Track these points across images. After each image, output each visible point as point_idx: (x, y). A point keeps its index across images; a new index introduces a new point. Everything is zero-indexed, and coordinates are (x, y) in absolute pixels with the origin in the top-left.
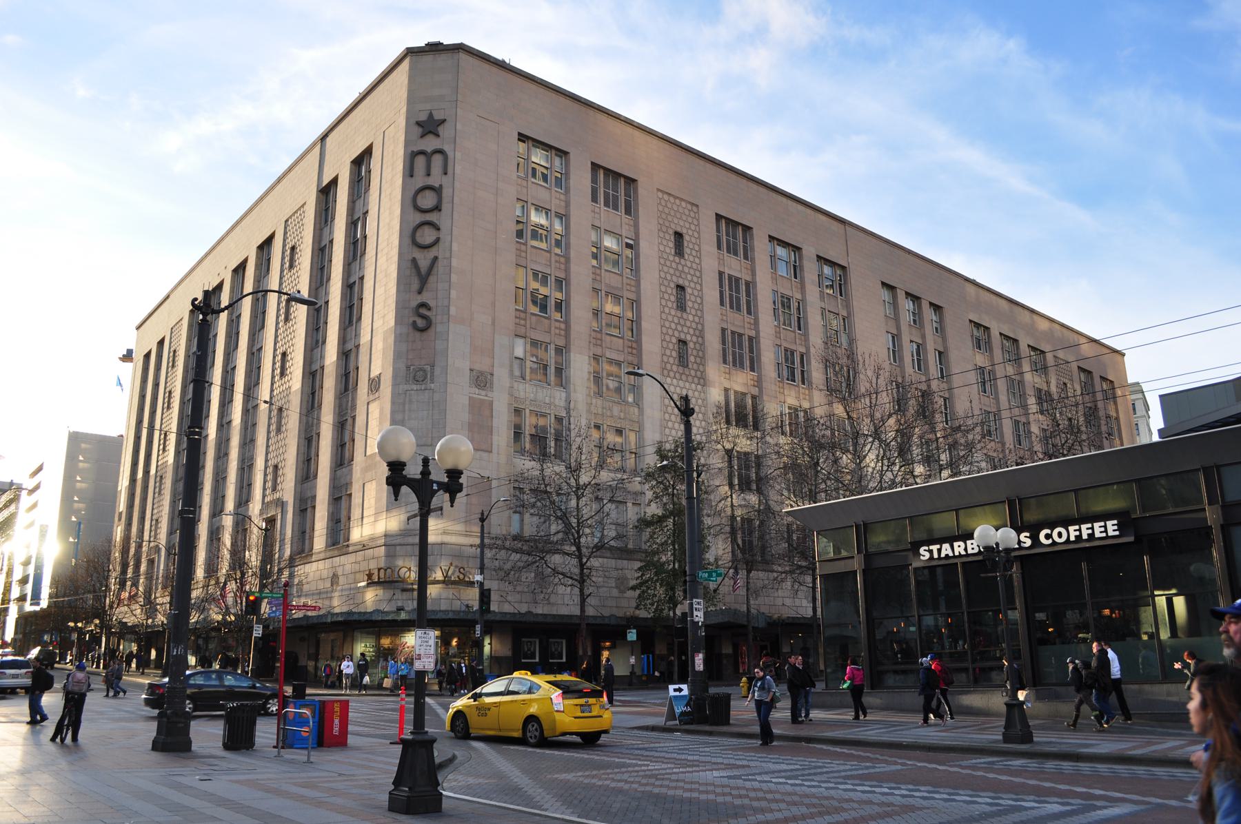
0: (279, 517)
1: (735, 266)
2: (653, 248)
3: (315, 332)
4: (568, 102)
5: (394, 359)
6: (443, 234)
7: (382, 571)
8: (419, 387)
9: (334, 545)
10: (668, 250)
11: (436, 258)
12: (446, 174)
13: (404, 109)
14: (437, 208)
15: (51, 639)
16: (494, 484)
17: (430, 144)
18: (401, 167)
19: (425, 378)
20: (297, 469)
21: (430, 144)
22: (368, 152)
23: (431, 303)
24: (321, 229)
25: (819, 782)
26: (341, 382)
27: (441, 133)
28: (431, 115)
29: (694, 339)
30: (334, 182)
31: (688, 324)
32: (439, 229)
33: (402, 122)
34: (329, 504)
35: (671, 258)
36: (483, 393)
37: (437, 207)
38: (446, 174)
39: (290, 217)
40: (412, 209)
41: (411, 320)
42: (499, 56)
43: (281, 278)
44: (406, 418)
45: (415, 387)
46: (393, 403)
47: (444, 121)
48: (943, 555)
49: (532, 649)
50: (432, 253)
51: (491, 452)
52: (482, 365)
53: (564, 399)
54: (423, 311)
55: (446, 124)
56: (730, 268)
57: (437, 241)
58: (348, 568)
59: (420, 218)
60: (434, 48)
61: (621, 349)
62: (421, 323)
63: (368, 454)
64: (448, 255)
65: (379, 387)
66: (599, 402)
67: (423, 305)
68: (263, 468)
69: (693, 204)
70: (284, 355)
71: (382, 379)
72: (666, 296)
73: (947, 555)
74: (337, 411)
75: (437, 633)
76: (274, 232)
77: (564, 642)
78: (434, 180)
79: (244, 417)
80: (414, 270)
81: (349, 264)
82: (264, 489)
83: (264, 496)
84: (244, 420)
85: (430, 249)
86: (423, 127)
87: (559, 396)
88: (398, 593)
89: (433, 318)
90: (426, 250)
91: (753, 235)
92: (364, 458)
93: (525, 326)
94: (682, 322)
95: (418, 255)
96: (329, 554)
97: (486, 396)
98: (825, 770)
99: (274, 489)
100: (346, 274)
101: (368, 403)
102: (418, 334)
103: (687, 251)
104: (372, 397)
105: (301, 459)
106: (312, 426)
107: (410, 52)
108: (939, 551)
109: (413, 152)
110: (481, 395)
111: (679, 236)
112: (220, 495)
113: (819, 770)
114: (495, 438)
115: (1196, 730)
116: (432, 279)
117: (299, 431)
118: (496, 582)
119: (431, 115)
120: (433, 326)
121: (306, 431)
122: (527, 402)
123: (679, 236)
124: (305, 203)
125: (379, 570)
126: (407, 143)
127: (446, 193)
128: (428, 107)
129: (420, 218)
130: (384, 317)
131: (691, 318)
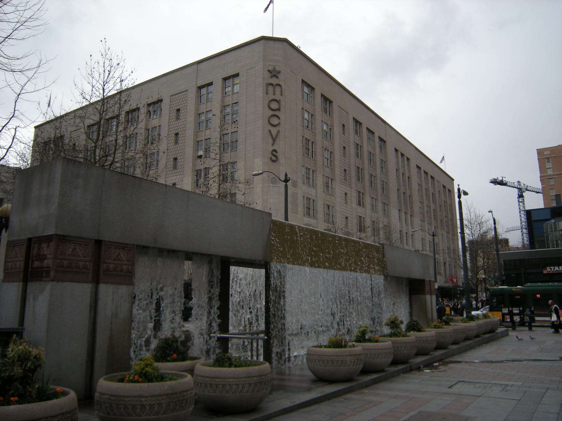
2: (337, 130)
4: (316, 69)
10: (341, 132)
14: (279, 109)
17: (274, 81)
21: (274, 81)
23: (278, 150)
27: (268, 73)
28: (274, 68)
32: (279, 119)
38: (281, 95)
42: (296, 44)
45: (272, 185)
48: (555, 270)
50: (276, 129)
51: (297, 213)
54: (274, 153)
62: (274, 158)
67: (275, 151)
73: (557, 270)
80: (269, 135)
86: (271, 73)
87: (314, 191)
95: (272, 129)
102: (274, 163)
103: (346, 132)
108: (554, 269)
111: (344, 125)
116: (278, 140)
119: (274, 68)
123: (344, 125)
127: (282, 103)
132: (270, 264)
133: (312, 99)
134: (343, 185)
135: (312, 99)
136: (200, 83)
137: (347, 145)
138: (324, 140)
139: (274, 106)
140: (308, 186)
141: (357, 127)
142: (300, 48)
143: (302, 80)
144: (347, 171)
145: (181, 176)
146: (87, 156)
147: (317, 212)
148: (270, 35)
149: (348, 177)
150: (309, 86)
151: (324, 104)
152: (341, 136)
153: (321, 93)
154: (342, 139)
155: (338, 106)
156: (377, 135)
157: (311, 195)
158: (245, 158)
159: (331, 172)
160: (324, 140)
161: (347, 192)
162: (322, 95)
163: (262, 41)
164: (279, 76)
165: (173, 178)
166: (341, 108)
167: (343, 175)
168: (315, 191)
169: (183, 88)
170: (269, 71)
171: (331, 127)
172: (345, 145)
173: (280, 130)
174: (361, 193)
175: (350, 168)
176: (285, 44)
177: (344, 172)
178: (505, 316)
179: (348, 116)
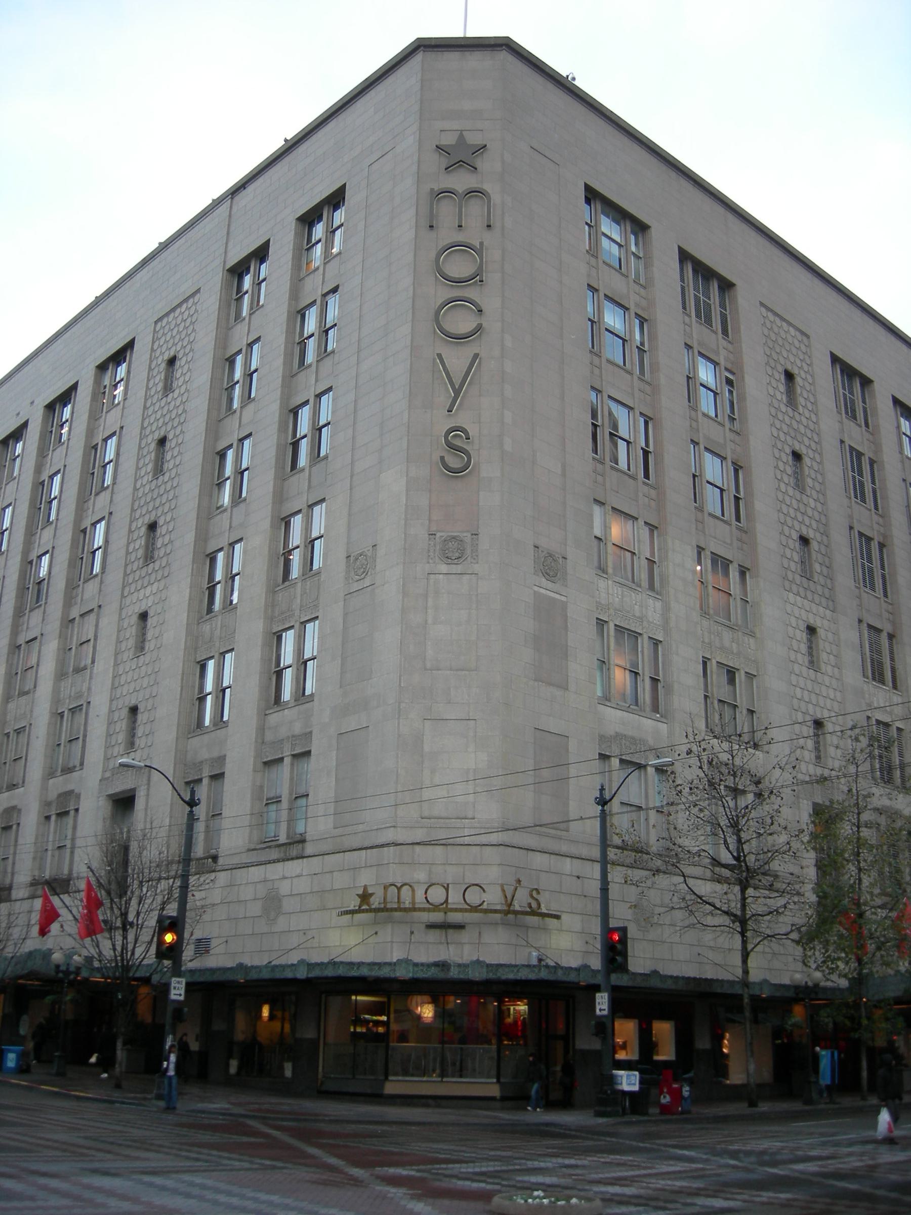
1: (856, 436)
10: (779, 396)
17: (461, 181)
23: (472, 431)
28: (461, 137)
29: (818, 535)
31: (810, 512)
35: (783, 409)
42: (562, 68)
44: (430, 621)
45: (444, 568)
51: (566, 689)
58: (303, 886)
61: (728, 541)
62: (454, 462)
66: (705, 623)
69: (803, 333)
72: (781, 465)
78: (474, 234)
87: (653, 609)
94: (802, 507)
99: (131, 744)
103: (801, 400)
109: (432, 190)
110: (546, 589)
111: (789, 376)
115: (385, 999)
119: (461, 137)
122: (612, 611)
123: (789, 376)
124: (198, 291)
127: (493, 255)
128: (456, 125)
132: (219, 836)
133: (641, 262)
134: (798, 594)
135: (641, 262)
136: (235, 257)
137: (809, 447)
138: (864, 595)
140: (630, 584)
142: (574, 79)
143: (588, 188)
144: (814, 545)
145: (163, 583)
147: (669, 690)
148: (455, 32)
149: (817, 567)
150: (620, 215)
152: (778, 409)
153: (680, 249)
155: (762, 304)
157: (641, 619)
158: (352, 477)
159: (739, 540)
160: (864, 595)
161: (817, 622)
163: (419, 57)
165: (148, 591)
167: (796, 557)
168: (659, 604)
169: (187, 288)
171: (733, 373)
172: (797, 447)
174: (884, 635)
175: (826, 534)
176: (504, 56)
177: (797, 544)
178: (767, 1075)
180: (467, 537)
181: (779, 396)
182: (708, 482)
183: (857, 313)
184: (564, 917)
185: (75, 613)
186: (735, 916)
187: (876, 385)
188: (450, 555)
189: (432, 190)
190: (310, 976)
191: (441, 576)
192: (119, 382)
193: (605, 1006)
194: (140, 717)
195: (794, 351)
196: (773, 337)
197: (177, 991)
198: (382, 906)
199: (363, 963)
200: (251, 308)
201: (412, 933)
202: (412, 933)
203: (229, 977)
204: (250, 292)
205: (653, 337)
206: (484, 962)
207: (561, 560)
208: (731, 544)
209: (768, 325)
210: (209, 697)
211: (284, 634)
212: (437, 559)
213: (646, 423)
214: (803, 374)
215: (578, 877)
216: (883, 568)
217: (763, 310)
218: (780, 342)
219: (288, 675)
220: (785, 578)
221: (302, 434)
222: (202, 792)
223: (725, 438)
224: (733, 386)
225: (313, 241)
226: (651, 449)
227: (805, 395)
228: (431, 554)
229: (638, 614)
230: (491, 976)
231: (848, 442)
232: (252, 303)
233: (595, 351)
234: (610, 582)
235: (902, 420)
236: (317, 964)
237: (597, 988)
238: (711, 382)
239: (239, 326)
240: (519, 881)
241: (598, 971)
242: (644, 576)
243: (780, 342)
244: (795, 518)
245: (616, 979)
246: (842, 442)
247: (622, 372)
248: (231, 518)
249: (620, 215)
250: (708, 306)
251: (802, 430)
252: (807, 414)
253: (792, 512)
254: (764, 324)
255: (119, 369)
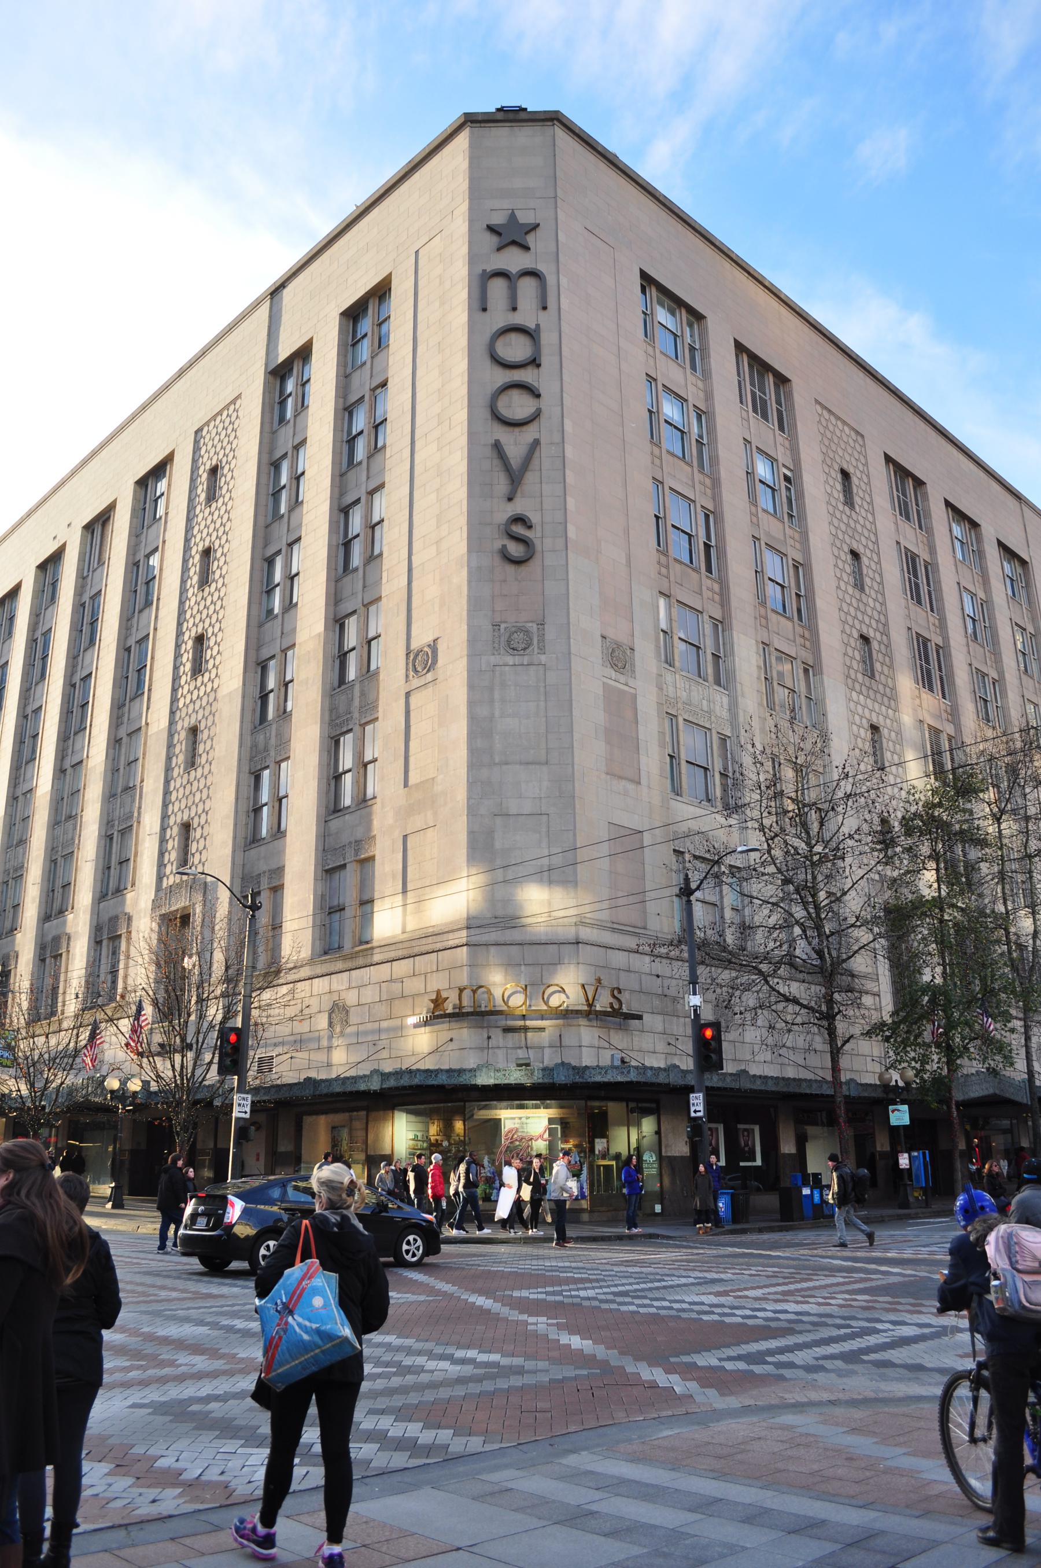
0: (198, 909)
3: (265, 595)
5: (469, 611)
6: (547, 402)
7: (467, 994)
8: (517, 660)
9: (326, 953)
10: (836, 495)
11: (536, 443)
12: (545, 308)
13: (465, 207)
14: (534, 362)
15: (1005, 1132)
16: (647, 838)
17: (514, 261)
18: (464, 295)
19: (529, 645)
20: (235, 825)
21: (514, 261)
22: (381, 292)
23: (534, 518)
24: (274, 432)
25: (713, 1313)
26: (333, 670)
27: (531, 245)
28: (513, 216)
29: (878, 635)
30: (304, 353)
31: (869, 611)
32: (538, 396)
33: (460, 227)
34: (316, 879)
35: (841, 507)
36: (622, 679)
37: (535, 360)
38: (545, 308)
39: (207, 424)
40: (487, 362)
41: (498, 544)
43: (189, 520)
44: (497, 713)
45: (510, 660)
46: (471, 687)
47: (536, 227)
49: (713, 1142)
50: (529, 434)
51: (639, 783)
52: (618, 633)
53: (726, 706)
54: (519, 529)
55: (539, 232)
56: (905, 537)
57: (536, 416)
59: (504, 376)
60: (511, 116)
61: (792, 638)
62: (515, 549)
63: (411, 782)
64: (557, 438)
65: (435, 661)
67: (520, 520)
68: (157, 828)
69: (857, 433)
70: (200, 639)
71: (441, 647)
74: (327, 718)
75: (552, 1112)
76: (115, 501)
77: (757, 1129)
78: (526, 316)
79: (111, 751)
80: (497, 462)
81: (342, 475)
82: (161, 865)
83: (160, 878)
84: (111, 758)
85: (524, 428)
86: (499, 234)
87: (720, 700)
88: (498, 1037)
89: (537, 543)
90: (517, 430)
91: (926, 493)
92: (401, 791)
93: (668, 577)
96: (319, 970)
97: (626, 685)
98: (664, 1284)
100: (337, 490)
101: (408, 695)
102: (511, 569)
103: (857, 500)
104: (416, 682)
105: (243, 808)
106: (266, 749)
107: (471, 120)
109: (484, 271)
110: (618, 682)
111: (845, 475)
112: (59, 883)
113: (657, 1284)
114: (643, 759)
116: (530, 478)
117: (240, 760)
118: (660, 1018)
119: (513, 216)
120: (538, 556)
121: (251, 760)
122: (680, 705)
123: (845, 475)
124: (239, 396)
125: (461, 990)
126: (473, 258)
127: (547, 339)
128: (506, 204)
129: (504, 376)
130: (438, 542)
131: (871, 602)
139: (516, 349)
141: (904, 494)
143: (644, 275)
146: (640, 896)
150: (675, 302)
151: (752, 384)
154: (840, 520)
155: (817, 402)
156: (989, 533)
162: (740, 348)
164: (530, 239)
166: (830, 411)
170: (491, 229)
173: (542, 441)
179: (864, 446)
180: (533, 627)
181: (836, 495)
182: (770, 579)
183: (909, 414)
184: (645, 1017)
185: (122, 733)
186: (821, 1013)
187: (929, 488)
188: (514, 646)
189: (484, 271)
190: (384, 1086)
191: (507, 668)
192: (160, 497)
193: (701, 1108)
194: (200, 737)
195: (850, 451)
196: (829, 435)
197: (241, 1108)
198: (457, 1010)
199: (442, 1070)
200: (296, 410)
201: (489, 1038)
202: (489, 1038)
203: (297, 1092)
204: (294, 394)
205: (712, 430)
206: (569, 1064)
207: (628, 652)
208: (794, 641)
209: (824, 423)
210: (265, 809)
211: (342, 739)
212: (502, 651)
213: (707, 516)
214: (858, 474)
215: (658, 976)
216: (940, 670)
217: (818, 408)
218: (836, 440)
219: (348, 780)
220: (848, 676)
221: (355, 534)
222: (264, 898)
223: (785, 534)
224: (790, 483)
225: (359, 336)
226: (713, 543)
227: (861, 494)
228: (496, 645)
229: (705, 708)
230: (578, 1079)
231: (903, 543)
232: (296, 405)
233: (654, 438)
234: (677, 676)
235: (954, 526)
236: (390, 1074)
237: (691, 1089)
238: (769, 478)
239: (283, 430)
240: (599, 980)
241: (690, 1072)
242: (710, 670)
243: (836, 440)
244: (855, 617)
245: (713, 1080)
246: (898, 543)
247: (682, 463)
248: (282, 624)
249: (675, 302)
250: (764, 402)
251: (859, 528)
252: (864, 513)
253: (852, 611)
254: (819, 422)
255: (159, 485)
